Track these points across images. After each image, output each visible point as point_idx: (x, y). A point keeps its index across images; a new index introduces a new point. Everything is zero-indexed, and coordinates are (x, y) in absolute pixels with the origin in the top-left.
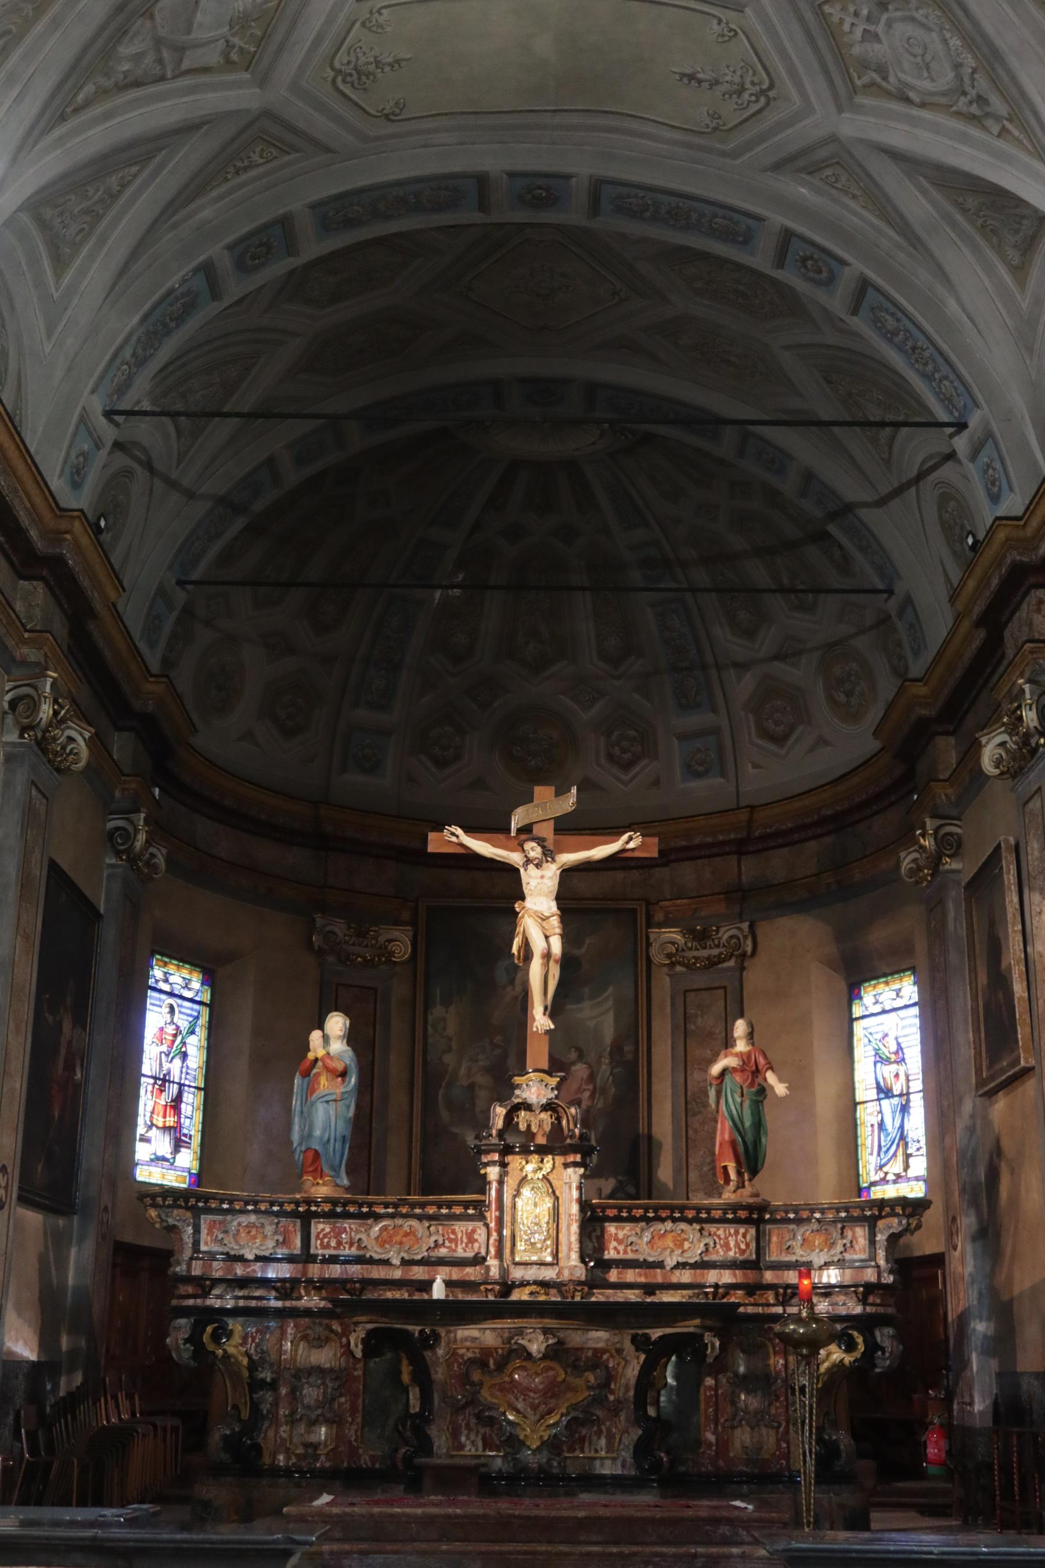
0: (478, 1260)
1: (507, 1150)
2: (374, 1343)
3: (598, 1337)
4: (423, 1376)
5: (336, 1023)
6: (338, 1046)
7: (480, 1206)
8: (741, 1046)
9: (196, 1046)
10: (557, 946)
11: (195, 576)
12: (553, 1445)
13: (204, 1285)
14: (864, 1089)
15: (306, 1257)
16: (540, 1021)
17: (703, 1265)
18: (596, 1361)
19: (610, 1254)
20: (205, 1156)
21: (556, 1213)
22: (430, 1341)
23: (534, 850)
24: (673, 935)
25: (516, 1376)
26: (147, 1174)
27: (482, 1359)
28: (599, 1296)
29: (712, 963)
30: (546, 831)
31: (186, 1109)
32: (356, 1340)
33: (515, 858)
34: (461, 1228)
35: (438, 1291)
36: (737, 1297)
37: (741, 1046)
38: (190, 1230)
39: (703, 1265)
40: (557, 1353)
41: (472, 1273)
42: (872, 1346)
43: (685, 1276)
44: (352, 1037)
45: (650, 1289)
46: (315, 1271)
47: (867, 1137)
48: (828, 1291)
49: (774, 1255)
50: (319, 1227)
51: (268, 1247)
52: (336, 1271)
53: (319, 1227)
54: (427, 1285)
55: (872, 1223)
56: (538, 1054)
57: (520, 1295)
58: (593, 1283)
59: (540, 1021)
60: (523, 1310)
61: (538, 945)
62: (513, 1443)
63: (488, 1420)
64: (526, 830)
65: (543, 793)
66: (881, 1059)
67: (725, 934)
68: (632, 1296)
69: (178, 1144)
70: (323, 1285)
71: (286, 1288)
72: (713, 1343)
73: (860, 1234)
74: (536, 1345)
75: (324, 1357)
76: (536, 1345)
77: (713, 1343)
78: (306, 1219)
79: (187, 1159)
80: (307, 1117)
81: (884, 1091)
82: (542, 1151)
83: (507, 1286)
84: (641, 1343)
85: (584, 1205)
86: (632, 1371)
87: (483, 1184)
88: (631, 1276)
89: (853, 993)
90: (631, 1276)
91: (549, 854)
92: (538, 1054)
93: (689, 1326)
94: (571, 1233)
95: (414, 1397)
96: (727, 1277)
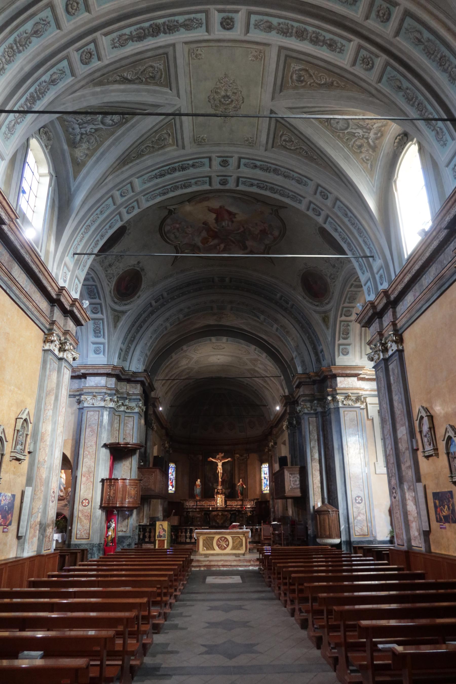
0: (214, 505)
1: (217, 494)
2: (204, 514)
3: (226, 513)
4: (209, 517)
5: (199, 480)
6: (199, 483)
7: (214, 500)
8: (241, 482)
9: (174, 473)
10: (222, 471)
11: (38, 106)
12: (222, 524)
13: (187, 509)
14: (263, 478)
15: (197, 505)
16: (220, 480)
17: (237, 505)
18: (226, 515)
19: (228, 504)
20: (176, 489)
21: (222, 500)
22: (210, 514)
23: (219, 461)
24: (238, 455)
25: (278, 408)
26: (170, 492)
27: (215, 515)
28: (226, 509)
29: (243, 459)
30: (220, 458)
31: (173, 482)
32: (203, 514)
33: (217, 461)
34: (212, 502)
35: (211, 509)
36: (240, 509)
37: (241, 482)
38: (213, 513)
39: (237, 505)
40: (222, 515)
41: (213, 507)
42: (253, 513)
43: (235, 507)
44: (200, 482)
45: (231, 508)
46: (198, 507)
47: (263, 484)
48: (248, 508)
49: (244, 504)
50: (198, 502)
51: (193, 504)
52: (200, 507)
53: (198, 502)
54: (209, 508)
55: (253, 501)
56: (220, 483)
57: (219, 509)
58: (226, 507)
59: (220, 480)
60: (219, 511)
61: (220, 471)
62: (218, 523)
63: (216, 522)
64: (218, 458)
65: (220, 454)
66: (265, 474)
67: (245, 455)
68: (230, 509)
69: (173, 487)
70: (199, 508)
71: (195, 509)
72: (237, 513)
73: (252, 502)
74: (220, 514)
75: (199, 516)
76: (220, 514)
77: (237, 513)
78: (197, 502)
79: (174, 489)
80: (196, 491)
81: (265, 478)
82: (220, 494)
83: (217, 508)
84: (230, 514)
85: (225, 499)
86: (229, 516)
87: (214, 498)
88: (230, 507)
89: (261, 465)
90: (230, 507)
91: (221, 461)
92: (220, 483)
93: (235, 512)
94: (223, 502)
95: (208, 519)
96: (239, 507)
